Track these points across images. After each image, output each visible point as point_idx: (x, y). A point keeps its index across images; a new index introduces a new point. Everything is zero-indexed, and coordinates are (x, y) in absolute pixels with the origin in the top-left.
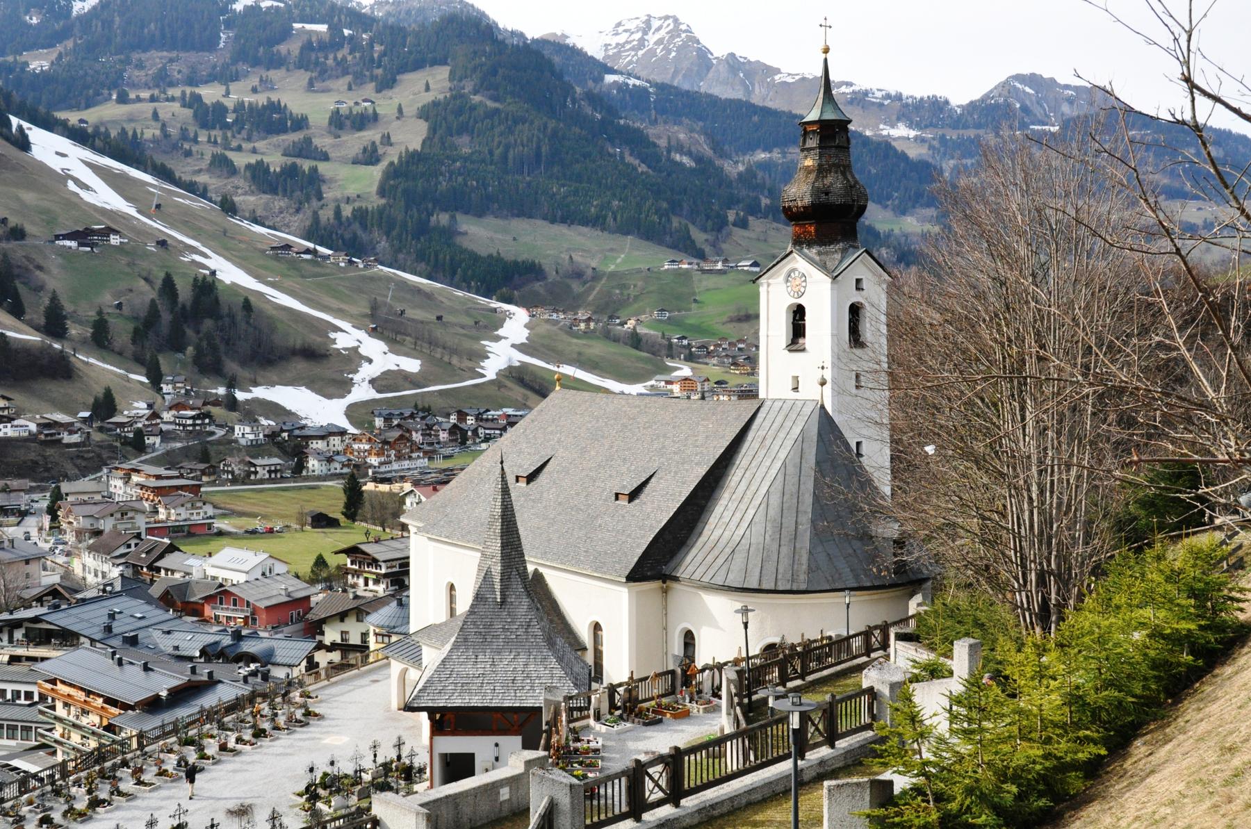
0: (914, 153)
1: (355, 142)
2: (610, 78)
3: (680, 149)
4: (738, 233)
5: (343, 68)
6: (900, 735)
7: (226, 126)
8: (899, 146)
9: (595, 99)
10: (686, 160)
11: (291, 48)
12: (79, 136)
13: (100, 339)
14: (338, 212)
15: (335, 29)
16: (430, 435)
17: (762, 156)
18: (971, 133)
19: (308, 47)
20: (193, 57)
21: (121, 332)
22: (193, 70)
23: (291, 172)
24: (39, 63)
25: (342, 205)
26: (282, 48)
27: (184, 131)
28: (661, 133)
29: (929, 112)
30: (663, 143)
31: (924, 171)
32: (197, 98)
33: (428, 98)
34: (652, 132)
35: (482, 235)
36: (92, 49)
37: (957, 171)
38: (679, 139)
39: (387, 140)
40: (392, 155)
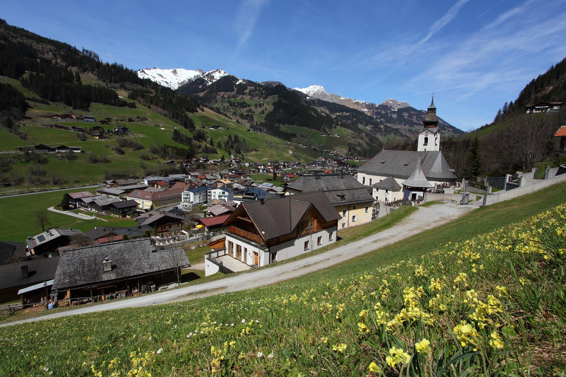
0: (369, 114)
1: (260, 110)
2: (308, 98)
3: (323, 112)
4: (334, 130)
5: (257, 95)
6: (229, 97)
7: (235, 106)
8: (366, 113)
9: (306, 102)
10: (324, 115)
11: (247, 91)
12: (212, 109)
13: (219, 146)
14: (257, 123)
15: (256, 88)
16: (275, 291)
17: (338, 114)
18: (380, 111)
19: (250, 91)
20: (228, 93)
21: (223, 146)
22: (229, 96)
23: (247, 115)
24: (201, 94)
25: (247, 109)
26: (245, 91)
27: (228, 107)
28: (319, 109)
29: (370, 106)
30: (319, 111)
31: (371, 118)
32: (230, 101)
33: (274, 101)
34: (317, 109)
35: (284, 128)
36: (210, 92)
37: (377, 118)
38: (323, 111)
39: (266, 109)
40: (266, 112)
